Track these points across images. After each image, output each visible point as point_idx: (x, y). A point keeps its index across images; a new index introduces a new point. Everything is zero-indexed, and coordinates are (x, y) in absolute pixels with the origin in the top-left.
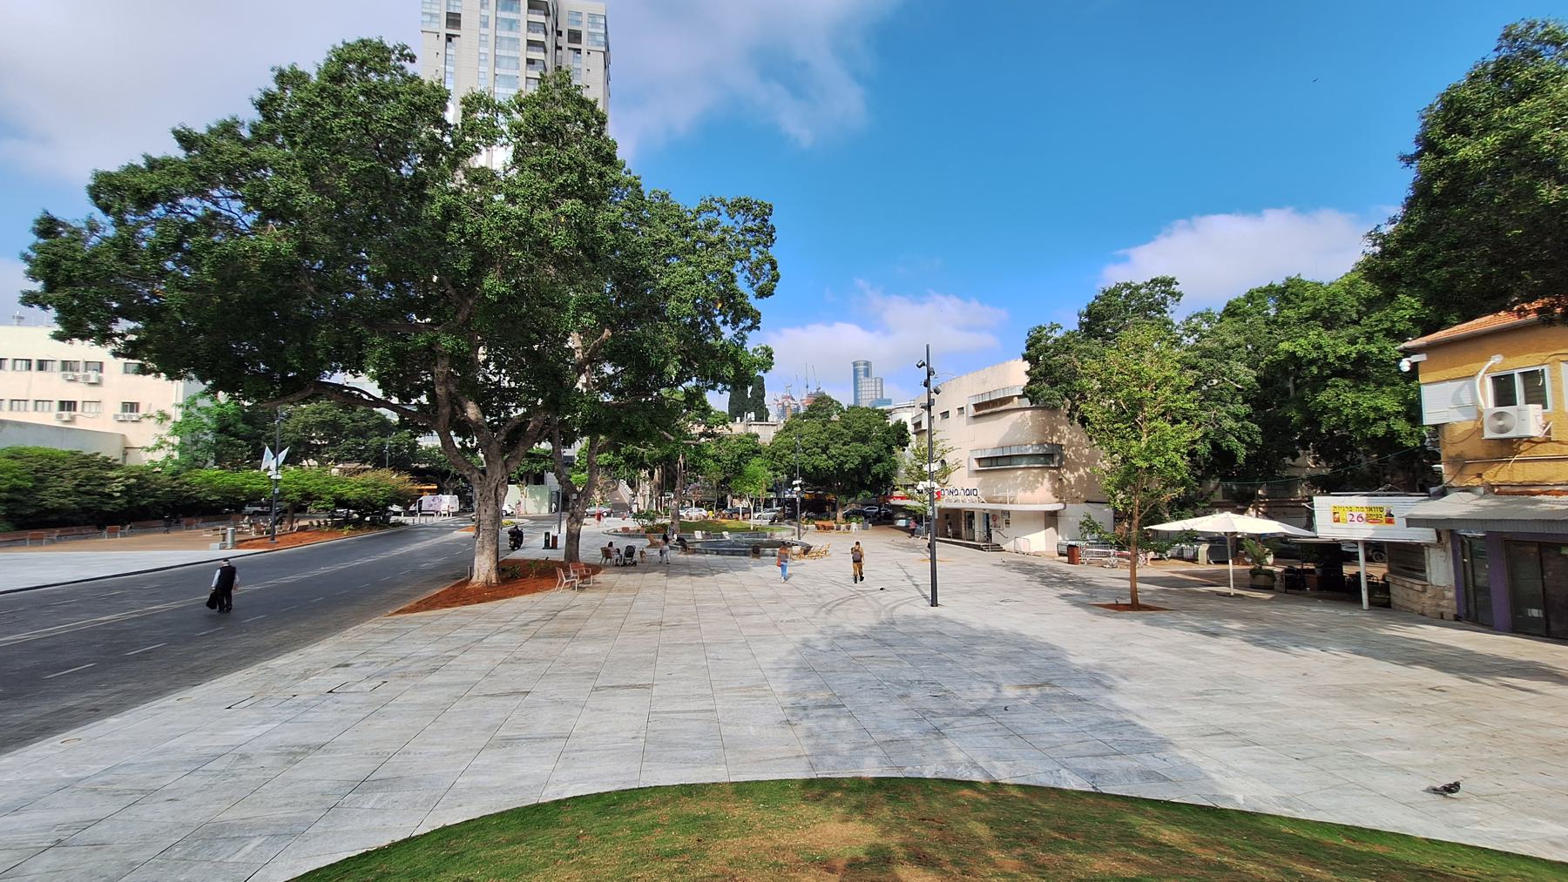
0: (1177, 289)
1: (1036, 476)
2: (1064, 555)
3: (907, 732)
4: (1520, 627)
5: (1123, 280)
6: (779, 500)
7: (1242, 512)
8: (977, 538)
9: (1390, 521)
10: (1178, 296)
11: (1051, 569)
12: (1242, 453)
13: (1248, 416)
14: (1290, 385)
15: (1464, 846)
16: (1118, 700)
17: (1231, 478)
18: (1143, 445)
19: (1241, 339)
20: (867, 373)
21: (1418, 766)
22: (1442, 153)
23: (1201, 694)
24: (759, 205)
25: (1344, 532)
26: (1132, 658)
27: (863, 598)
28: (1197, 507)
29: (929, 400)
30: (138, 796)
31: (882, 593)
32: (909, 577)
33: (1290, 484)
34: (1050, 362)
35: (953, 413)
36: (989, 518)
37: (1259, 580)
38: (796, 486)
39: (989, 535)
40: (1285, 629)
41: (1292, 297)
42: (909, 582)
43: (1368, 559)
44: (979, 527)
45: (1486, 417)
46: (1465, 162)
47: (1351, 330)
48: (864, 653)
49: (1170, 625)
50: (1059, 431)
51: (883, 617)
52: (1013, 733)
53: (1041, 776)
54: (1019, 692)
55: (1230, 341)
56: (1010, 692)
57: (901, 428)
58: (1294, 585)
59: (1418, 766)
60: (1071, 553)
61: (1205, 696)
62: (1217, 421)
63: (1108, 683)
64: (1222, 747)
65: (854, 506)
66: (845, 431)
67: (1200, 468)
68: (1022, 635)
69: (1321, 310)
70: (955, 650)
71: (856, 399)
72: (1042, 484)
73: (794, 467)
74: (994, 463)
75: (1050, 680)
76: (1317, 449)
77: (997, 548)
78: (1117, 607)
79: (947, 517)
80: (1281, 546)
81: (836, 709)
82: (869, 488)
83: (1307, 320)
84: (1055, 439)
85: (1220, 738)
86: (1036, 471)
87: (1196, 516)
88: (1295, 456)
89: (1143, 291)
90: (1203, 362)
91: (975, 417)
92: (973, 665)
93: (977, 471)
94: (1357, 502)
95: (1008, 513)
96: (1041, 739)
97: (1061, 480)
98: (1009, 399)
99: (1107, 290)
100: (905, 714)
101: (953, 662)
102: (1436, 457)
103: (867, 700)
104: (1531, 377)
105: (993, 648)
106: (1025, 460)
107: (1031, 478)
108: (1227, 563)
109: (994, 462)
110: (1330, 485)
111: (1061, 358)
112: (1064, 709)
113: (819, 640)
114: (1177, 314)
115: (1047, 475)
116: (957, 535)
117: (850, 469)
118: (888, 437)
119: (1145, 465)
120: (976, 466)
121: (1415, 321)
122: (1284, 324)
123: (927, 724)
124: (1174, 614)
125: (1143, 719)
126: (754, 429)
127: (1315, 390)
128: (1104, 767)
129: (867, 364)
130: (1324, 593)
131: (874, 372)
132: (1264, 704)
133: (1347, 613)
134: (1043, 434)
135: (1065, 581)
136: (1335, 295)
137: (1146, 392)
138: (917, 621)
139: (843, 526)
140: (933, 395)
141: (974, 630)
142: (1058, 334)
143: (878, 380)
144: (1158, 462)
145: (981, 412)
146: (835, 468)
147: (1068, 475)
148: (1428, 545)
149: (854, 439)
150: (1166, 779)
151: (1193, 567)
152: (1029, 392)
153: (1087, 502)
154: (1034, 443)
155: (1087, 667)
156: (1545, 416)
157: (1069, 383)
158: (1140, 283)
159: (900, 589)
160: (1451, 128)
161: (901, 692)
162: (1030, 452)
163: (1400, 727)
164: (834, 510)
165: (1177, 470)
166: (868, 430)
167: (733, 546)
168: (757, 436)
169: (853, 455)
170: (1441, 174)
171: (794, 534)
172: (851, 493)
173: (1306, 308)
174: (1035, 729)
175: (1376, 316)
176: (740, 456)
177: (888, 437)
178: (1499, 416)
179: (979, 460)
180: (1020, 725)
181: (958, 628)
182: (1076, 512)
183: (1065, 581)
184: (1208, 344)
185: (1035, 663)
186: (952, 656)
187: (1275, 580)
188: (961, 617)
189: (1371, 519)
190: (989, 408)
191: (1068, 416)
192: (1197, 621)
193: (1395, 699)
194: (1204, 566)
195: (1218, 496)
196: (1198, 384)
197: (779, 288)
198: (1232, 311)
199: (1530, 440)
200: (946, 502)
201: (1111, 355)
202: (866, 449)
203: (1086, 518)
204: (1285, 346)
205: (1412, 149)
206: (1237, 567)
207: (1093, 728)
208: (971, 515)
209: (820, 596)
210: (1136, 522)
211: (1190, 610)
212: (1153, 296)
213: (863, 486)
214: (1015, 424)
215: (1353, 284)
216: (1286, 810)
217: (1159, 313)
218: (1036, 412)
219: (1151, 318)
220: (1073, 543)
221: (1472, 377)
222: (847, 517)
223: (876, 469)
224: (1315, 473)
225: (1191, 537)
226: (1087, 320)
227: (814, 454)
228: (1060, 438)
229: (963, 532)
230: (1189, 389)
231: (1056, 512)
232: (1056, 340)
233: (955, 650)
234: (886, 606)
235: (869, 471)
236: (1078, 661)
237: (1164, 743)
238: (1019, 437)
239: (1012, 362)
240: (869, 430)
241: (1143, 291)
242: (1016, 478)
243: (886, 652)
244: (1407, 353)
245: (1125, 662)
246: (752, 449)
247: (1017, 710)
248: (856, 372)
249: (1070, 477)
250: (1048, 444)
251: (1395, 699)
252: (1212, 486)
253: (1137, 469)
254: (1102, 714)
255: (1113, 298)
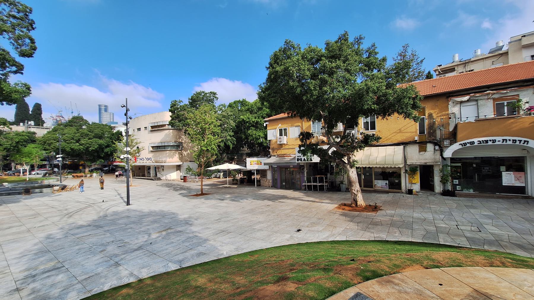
0: (217, 96)
1: (174, 153)
2: (183, 180)
3: (100, 269)
4: (282, 188)
5: (202, 90)
6: (51, 165)
7: (231, 163)
8: (151, 176)
9: (261, 164)
10: (217, 98)
11: (178, 185)
12: (231, 146)
13: (233, 136)
14: (243, 128)
15: (273, 247)
16: (194, 229)
17: (229, 154)
18: (205, 143)
19: (232, 113)
20: (106, 110)
21: (265, 228)
22: (273, 68)
23: (218, 220)
24: (22, 5)
25: (252, 167)
26: (199, 212)
27: (92, 207)
28: (220, 162)
29: (127, 121)
30: (79, 238)
31: (103, 203)
32: (119, 194)
33: (242, 155)
34: (178, 113)
35: (143, 129)
36: (156, 168)
37: (235, 182)
38: (59, 158)
39: (156, 175)
40: (240, 195)
41: (244, 104)
42: (119, 197)
43: (257, 174)
44: (152, 172)
45: (278, 138)
46: (277, 71)
47: (255, 115)
48: (85, 234)
49: (211, 199)
50: (182, 138)
51: (102, 214)
52: (153, 254)
53: (159, 268)
54: (158, 235)
55: (230, 114)
56: (154, 236)
57: (120, 133)
58: (241, 182)
59: (265, 228)
60: (184, 179)
61: (218, 220)
62: (226, 137)
63: (191, 223)
64: (222, 236)
65: (96, 166)
66: (90, 133)
67: (221, 150)
68: (163, 211)
69: (250, 108)
70: (134, 222)
71: (100, 120)
72: (175, 156)
73: (58, 149)
74: (158, 148)
75: (171, 227)
76: (248, 146)
77: (159, 179)
78: (197, 195)
79: (140, 169)
80: (239, 171)
81: (57, 270)
82: (103, 158)
83: (247, 111)
84: (180, 140)
85: (222, 233)
86: (173, 151)
87: (220, 165)
88: (243, 147)
89: (208, 95)
90: (223, 119)
91: (151, 131)
92: (141, 228)
93: (152, 151)
94: (255, 159)
95: (163, 166)
96: (163, 252)
97: (182, 154)
98: (164, 125)
99: (197, 92)
100: (101, 260)
101: (131, 228)
102: (269, 148)
103: (80, 259)
104: (285, 130)
105: (151, 219)
106: (170, 147)
107: (172, 154)
108: (227, 178)
109: (159, 148)
110: (250, 155)
111: (182, 113)
112: (174, 237)
113: (58, 233)
114: (217, 103)
115: (177, 153)
116: (144, 175)
117: (93, 150)
118: (113, 137)
119: (206, 149)
120: (151, 149)
121: (267, 114)
122: (242, 111)
123: (112, 262)
124: (213, 195)
125: (200, 233)
126: (32, 130)
127: (248, 130)
128: (185, 257)
129: (106, 106)
130: (248, 184)
131: (110, 110)
132: (234, 219)
133: (252, 189)
134: (177, 139)
135: (182, 188)
136: (252, 105)
137: (207, 126)
138: (118, 213)
139: (89, 175)
140: (129, 120)
141: (144, 212)
142: (182, 104)
143: (111, 114)
144: (209, 148)
145: (154, 129)
146: (84, 150)
147: (184, 153)
148: (267, 170)
149: (94, 137)
150: (205, 254)
151: (219, 180)
152: (171, 123)
153: (190, 161)
154: (173, 141)
155: (185, 218)
156: (287, 139)
157: (185, 121)
158: (207, 92)
159: (114, 200)
160: (275, 62)
161: (101, 249)
162: (172, 144)
163: (261, 218)
164: (85, 168)
165: (214, 151)
166: (102, 133)
167: (11, 190)
168: (34, 133)
169: (95, 144)
170: (273, 73)
171: (58, 181)
172: (93, 161)
173: (247, 107)
174: (161, 249)
175: (260, 112)
176: (17, 143)
177: (113, 137)
178: (280, 138)
179: (153, 147)
180: (155, 249)
181: (137, 213)
182: (186, 165)
183: (182, 188)
184: (224, 113)
185: (166, 221)
186: (132, 226)
187: (238, 181)
188: (139, 208)
189: (258, 164)
190: (157, 128)
191: (184, 132)
192: (219, 196)
193: (260, 210)
194: (222, 179)
195: (226, 159)
196: (220, 126)
197: (36, 54)
198: (230, 106)
199: (284, 144)
200: (139, 163)
201: (197, 112)
202: (101, 141)
203: (188, 167)
204: (242, 117)
205: (268, 66)
206: (230, 179)
207: (183, 242)
208: (149, 168)
209: (66, 210)
210: (203, 167)
211: (216, 193)
212: (210, 97)
213: (99, 157)
214: (166, 134)
215: (256, 103)
216: (236, 252)
217: (212, 103)
218: (174, 131)
219: (210, 104)
220: (185, 175)
221: (276, 129)
222: (92, 171)
223: (106, 150)
224: (247, 152)
225: (219, 171)
226: (191, 101)
227: (71, 143)
228: (182, 140)
229: (146, 174)
230: (219, 126)
231: (180, 165)
232: (181, 106)
233: (134, 222)
234: (104, 209)
235: (103, 151)
236: (182, 217)
237: (206, 240)
238: (168, 139)
239: (166, 112)
240: (103, 134)
241: (208, 95)
242: (167, 154)
243: (100, 231)
244: (265, 122)
245: (197, 214)
246: (31, 139)
247: (156, 242)
248: (100, 110)
249: (185, 153)
250: (178, 142)
251: (260, 210)
252: (224, 156)
253: (204, 150)
254: (187, 235)
255: (199, 95)
